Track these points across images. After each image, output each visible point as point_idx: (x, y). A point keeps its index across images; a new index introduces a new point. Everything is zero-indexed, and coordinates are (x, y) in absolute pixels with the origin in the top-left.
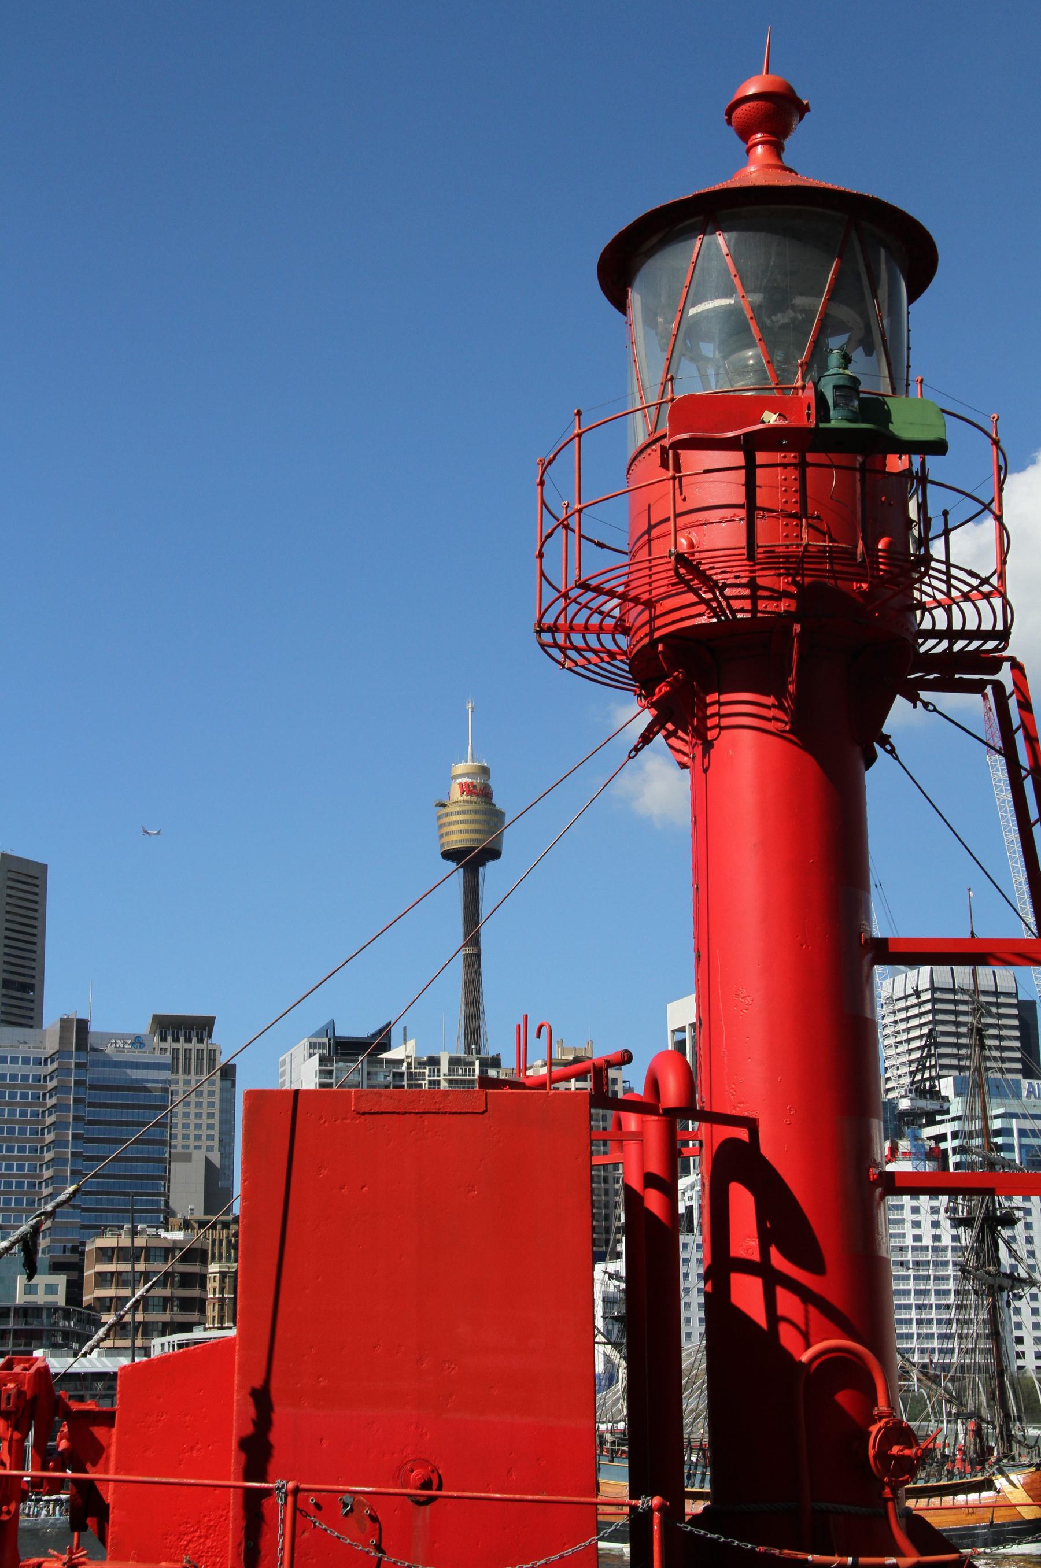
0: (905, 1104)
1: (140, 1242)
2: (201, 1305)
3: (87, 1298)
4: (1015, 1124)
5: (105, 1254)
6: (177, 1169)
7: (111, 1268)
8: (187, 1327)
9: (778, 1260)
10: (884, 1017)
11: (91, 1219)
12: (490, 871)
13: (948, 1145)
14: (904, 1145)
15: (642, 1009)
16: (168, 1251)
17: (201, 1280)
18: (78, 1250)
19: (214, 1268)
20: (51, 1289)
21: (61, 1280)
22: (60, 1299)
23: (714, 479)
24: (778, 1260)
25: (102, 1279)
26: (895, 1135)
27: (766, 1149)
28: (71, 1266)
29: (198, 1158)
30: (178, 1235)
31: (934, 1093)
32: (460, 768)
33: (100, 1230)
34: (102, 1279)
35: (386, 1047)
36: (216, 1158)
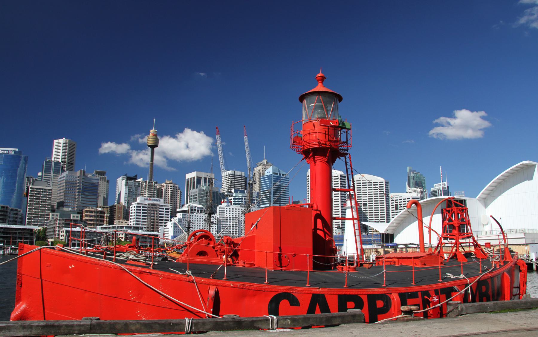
0: (226, 193)
1: (93, 210)
2: (103, 221)
3: (84, 219)
4: (243, 198)
5: (87, 211)
6: (99, 198)
7: (88, 214)
8: (102, 225)
9: (325, 230)
10: (223, 178)
11: (84, 205)
12: (156, 149)
13: (233, 200)
14: (225, 200)
15: (306, 198)
16: (98, 212)
17: (104, 217)
18: (82, 210)
19: (105, 215)
20: (77, 217)
21: (79, 215)
22: (79, 218)
23: (344, 139)
24: (325, 230)
25: (87, 216)
26: (224, 198)
27: (322, 215)
28: (81, 213)
29: (102, 196)
30: (100, 209)
31: (231, 192)
32: (151, 131)
33: (86, 207)
34: (87, 216)
35: (136, 179)
36: (105, 196)
